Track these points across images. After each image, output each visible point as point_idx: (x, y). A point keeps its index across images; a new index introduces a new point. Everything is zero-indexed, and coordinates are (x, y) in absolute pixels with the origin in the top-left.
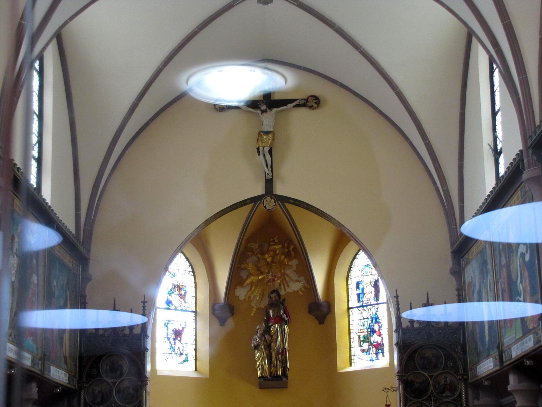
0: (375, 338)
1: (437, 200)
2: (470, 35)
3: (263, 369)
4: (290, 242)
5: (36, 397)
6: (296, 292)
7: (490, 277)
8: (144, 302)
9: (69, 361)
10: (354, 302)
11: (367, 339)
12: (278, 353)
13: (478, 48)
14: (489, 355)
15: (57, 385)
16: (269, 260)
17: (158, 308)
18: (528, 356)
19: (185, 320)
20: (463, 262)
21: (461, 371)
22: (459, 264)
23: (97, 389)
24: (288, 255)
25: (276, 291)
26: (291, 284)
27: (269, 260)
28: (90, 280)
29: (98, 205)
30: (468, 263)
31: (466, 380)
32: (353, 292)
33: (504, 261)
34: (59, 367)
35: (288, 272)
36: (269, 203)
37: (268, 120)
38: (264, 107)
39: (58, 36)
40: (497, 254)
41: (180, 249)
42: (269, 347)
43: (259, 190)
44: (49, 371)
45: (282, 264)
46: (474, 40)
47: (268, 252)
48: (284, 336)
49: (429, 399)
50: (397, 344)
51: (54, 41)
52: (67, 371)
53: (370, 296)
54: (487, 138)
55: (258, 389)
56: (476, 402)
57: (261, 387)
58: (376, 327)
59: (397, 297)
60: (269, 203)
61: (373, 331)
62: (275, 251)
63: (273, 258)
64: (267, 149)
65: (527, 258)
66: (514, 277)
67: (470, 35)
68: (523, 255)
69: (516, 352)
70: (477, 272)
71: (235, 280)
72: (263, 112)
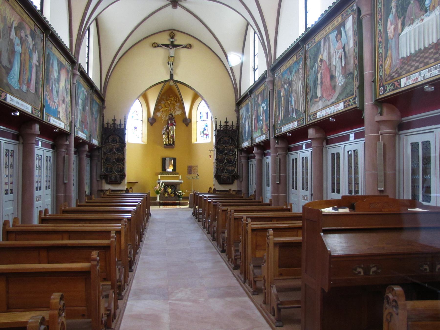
0: (206, 132)
1: (231, 84)
2: (248, 24)
3: (166, 141)
4: (177, 97)
5: (88, 150)
6: (178, 115)
7: (250, 113)
8: (125, 117)
10: (199, 119)
11: (203, 132)
12: (171, 136)
14: (247, 140)
16: (169, 103)
18: (262, 142)
19: (139, 124)
20: (240, 108)
21: (236, 145)
22: (238, 108)
23: (108, 147)
24: (176, 101)
25: (171, 114)
26: (177, 112)
27: (169, 103)
30: (241, 108)
31: (238, 148)
32: (199, 116)
33: (256, 109)
34: (95, 139)
35: (176, 107)
36: (172, 83)
37: (172, 52)
38: (171, 47)
39: (96, 19)
40: (253, 106)
41: (138, 98)
42: (168, 134)
43: (168, 78)
45: (174, 105)
46: (249, 25)
47: (169, 100)
48: (173, 131)
49: (225, 154)
50: (215, 135)
51: (95, 21)
52: (98, 141)
53: (204, 117)
54: (252, 65)
55: (163, 148)
56: (241, 156)
57: (165, 148)
58: (206, 128)
59: (216, 119)
60: (172, 83)
61: (205, 130)
62: (171, 100)
63: (171, 102)
64: (171, 63)
65: (265, 108)
66: (259, 114)
67: (248, 24)
68: (263, 107)
69: (258, 140)
70: (245, 112)
71: (157, 109)
72: (170, 49)
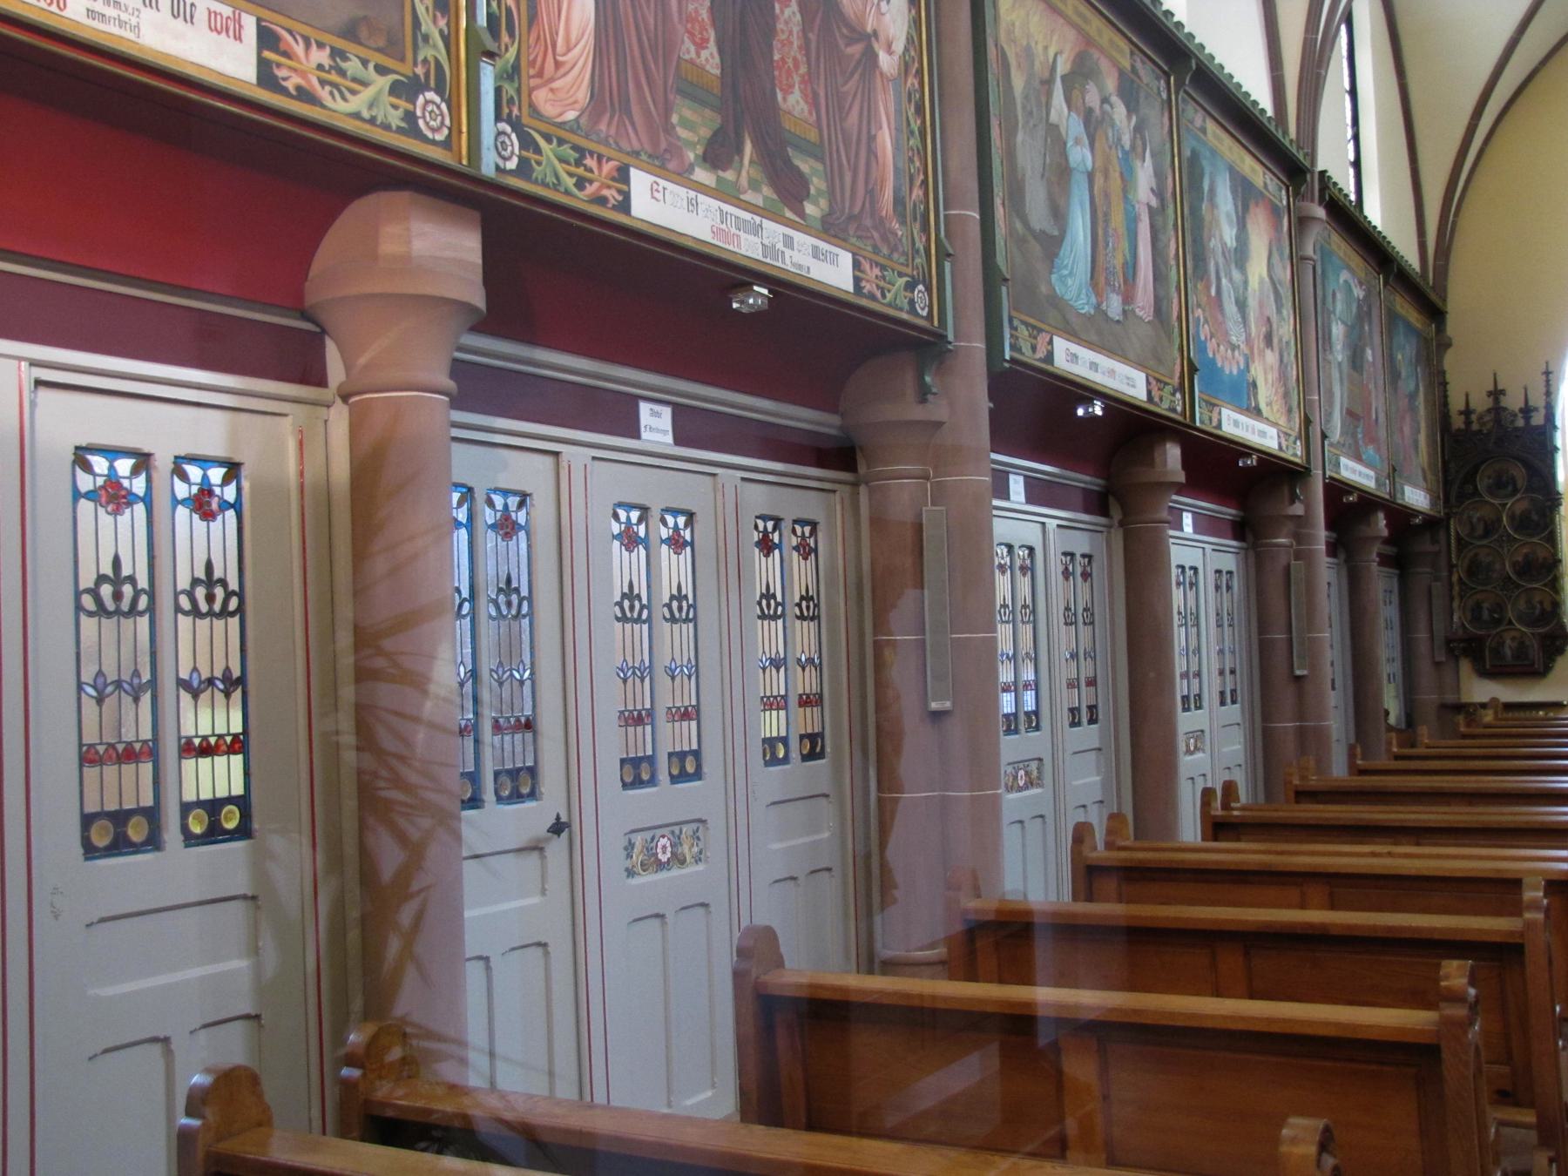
5: (1385, 533)
9: (1429, 476)
13: (1383, 218)
15: (1414, 513)
17: (543, 858)
28: (1449, 345)
29: (1454, 223)
34: (1415, 485)
44: (1403, 493)
52: (1428, 490)
